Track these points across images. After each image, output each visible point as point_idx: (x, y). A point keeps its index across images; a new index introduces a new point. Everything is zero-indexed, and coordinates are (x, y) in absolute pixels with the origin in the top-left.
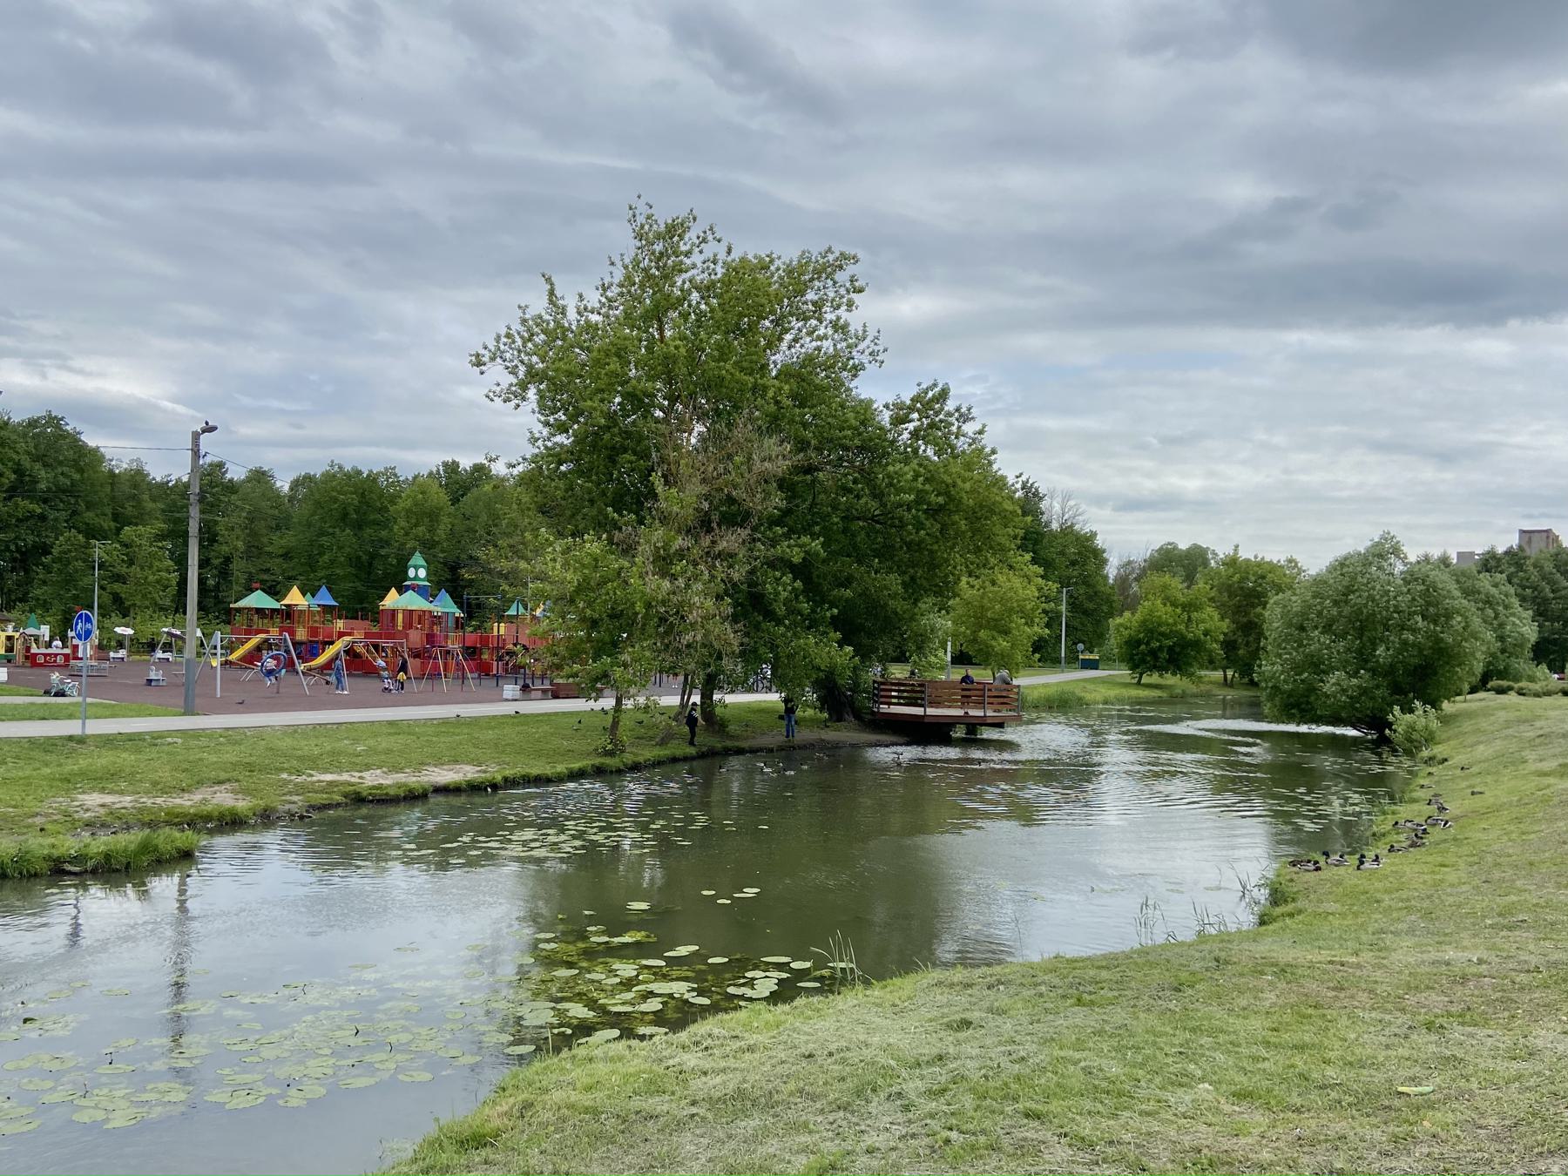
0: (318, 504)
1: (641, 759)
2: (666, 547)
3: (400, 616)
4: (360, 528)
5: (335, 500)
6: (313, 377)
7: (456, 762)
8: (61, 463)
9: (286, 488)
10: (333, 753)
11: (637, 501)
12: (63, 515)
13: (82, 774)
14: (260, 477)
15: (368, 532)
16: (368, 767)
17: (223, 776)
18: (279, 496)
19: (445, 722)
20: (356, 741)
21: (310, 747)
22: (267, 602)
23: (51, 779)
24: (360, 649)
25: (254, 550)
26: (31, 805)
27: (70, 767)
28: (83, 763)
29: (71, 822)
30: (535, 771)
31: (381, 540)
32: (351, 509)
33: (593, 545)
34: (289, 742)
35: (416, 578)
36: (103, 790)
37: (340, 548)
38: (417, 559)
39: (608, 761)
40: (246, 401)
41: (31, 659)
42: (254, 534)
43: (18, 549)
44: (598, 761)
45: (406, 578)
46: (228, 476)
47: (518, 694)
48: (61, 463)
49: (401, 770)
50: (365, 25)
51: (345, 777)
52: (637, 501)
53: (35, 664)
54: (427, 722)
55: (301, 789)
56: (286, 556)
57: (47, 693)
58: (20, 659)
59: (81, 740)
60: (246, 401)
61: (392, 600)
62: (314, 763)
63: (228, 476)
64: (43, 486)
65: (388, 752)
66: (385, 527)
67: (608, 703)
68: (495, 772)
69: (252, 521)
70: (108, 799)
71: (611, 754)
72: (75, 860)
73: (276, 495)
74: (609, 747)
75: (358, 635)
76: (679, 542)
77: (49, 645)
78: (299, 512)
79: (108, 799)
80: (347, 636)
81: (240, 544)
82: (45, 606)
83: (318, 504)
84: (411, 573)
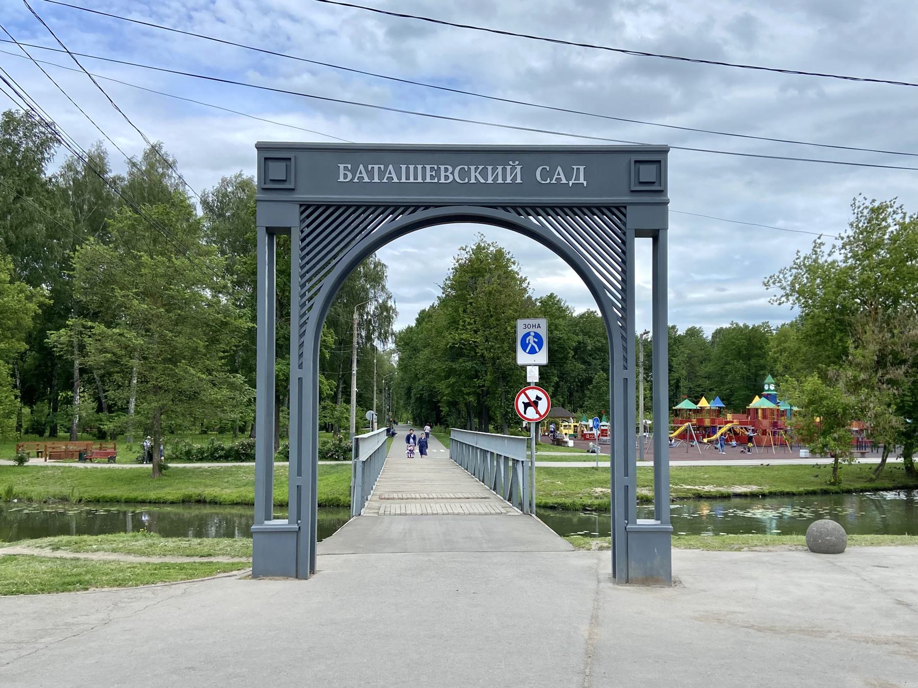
0: (724, 346)
1: (852, 488)
2: (855, 378)
3: (760, 411)
4: (749, 359)
5: (733, 343)
6: (737, 257)
7: (750, 484)
8: (597, 335)
9: (710, 338)
10: (694, 478)
11: (840, 357)
12: (598, 362)
13: (596, 481)
14: (693, 333)
15: (753, 361)
16: (707, 484)
17: (646, 484)
18: (705, 343)
19: (756, 467)
20: (706, 473)
21: (684, 475)
22: (692, 406)
23: (585, 482)
24: (738, 429)
25: (692, 375)
26: (578, 490)
27: (592, 478)
28: (596, 477)
29: (590, 496)
30: (787, 490)
31: (760, 366)
32: (743, 349)
33: (812, 381)
34: (677, 472)
35: (769, 390)
36: (602, 487)
37: (736, 372)
38: (769, 379)
39: (832, 488)
40: (698, 277)
41: (584, 435)
42: (692, 366)
43: (579, 381)
44: (825, 487)
45: (763, 390)
46: (678, 333)
47: (808, 455)
48: (597, 335)
49: (722, 486)
50: (745, 29)
51: (697, 487)
52: (840, 357)
53: (586, 439)
54: (745, 467)
55: (676, 491)
56: (708, 377)
57: (588, 451)
58: (579, 436)
59: (596, 469)
60: (698, 277)
61: (758, 402)
62: (684, 481)
63: (678, 333)
64: (589, 348)
65: (718, 478)
66: (763, 358)
67: (878, 460)
68: (766, 489)
69: (690, 358)
70: (604, 490)
71: (833, 484)
72: (589, 506)
73: (704, 341)
74: (833, 480)
75: (736, 422)
76: (863, 376)
77: (591, 429)
78: (716, 351)
79: (604, 490)
80: (732, 420)
81: (684, 372)
82: (591, 409)
83: (724, 346)
84: (766, 387)
